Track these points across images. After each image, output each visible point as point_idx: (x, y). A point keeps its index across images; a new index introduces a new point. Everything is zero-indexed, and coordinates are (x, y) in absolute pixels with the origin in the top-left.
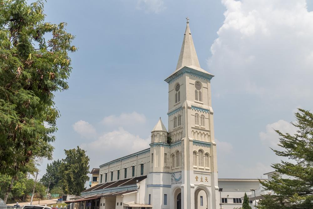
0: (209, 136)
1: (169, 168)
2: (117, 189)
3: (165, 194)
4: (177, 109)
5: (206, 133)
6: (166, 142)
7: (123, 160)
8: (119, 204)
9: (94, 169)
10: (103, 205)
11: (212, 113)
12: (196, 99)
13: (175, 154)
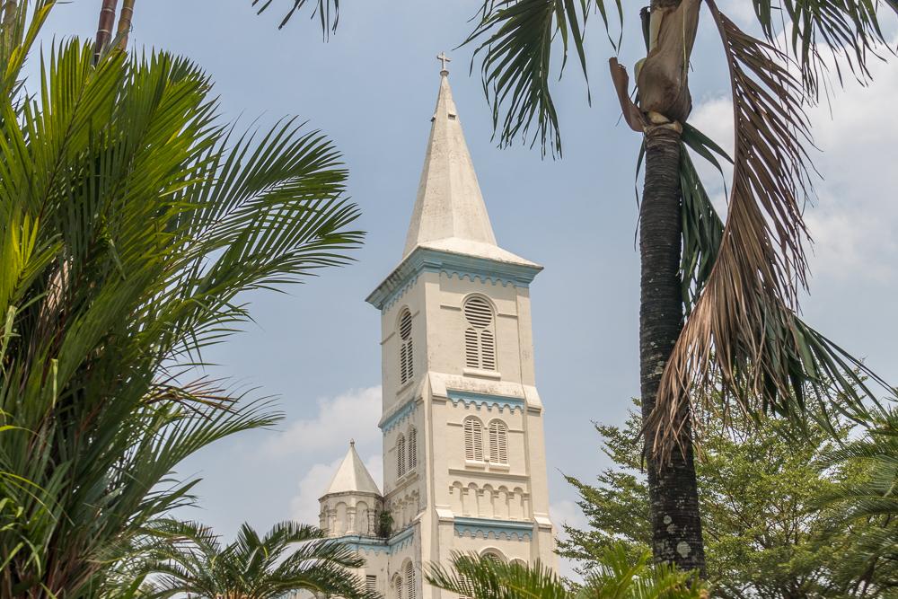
0: (526, 496)
4: (405, 407)
5: (511, 486)
6: (373, 534)
11: (535, 411)
12: (472, 362)
13: (403, 575)
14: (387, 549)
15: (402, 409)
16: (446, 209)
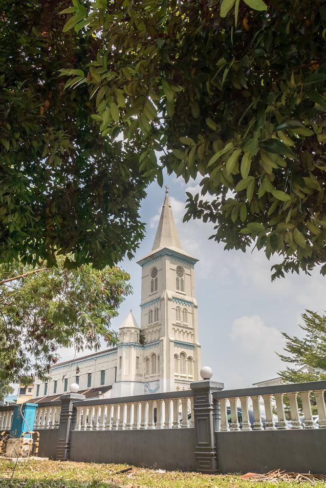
0: (193, 335)
4: (154, 300)
5: (189, 331)
6: (139, 342)
11: (196, 307)
12: (178, 288)
13: (150, 358)
15: (151, 301)
16: (169, 236)
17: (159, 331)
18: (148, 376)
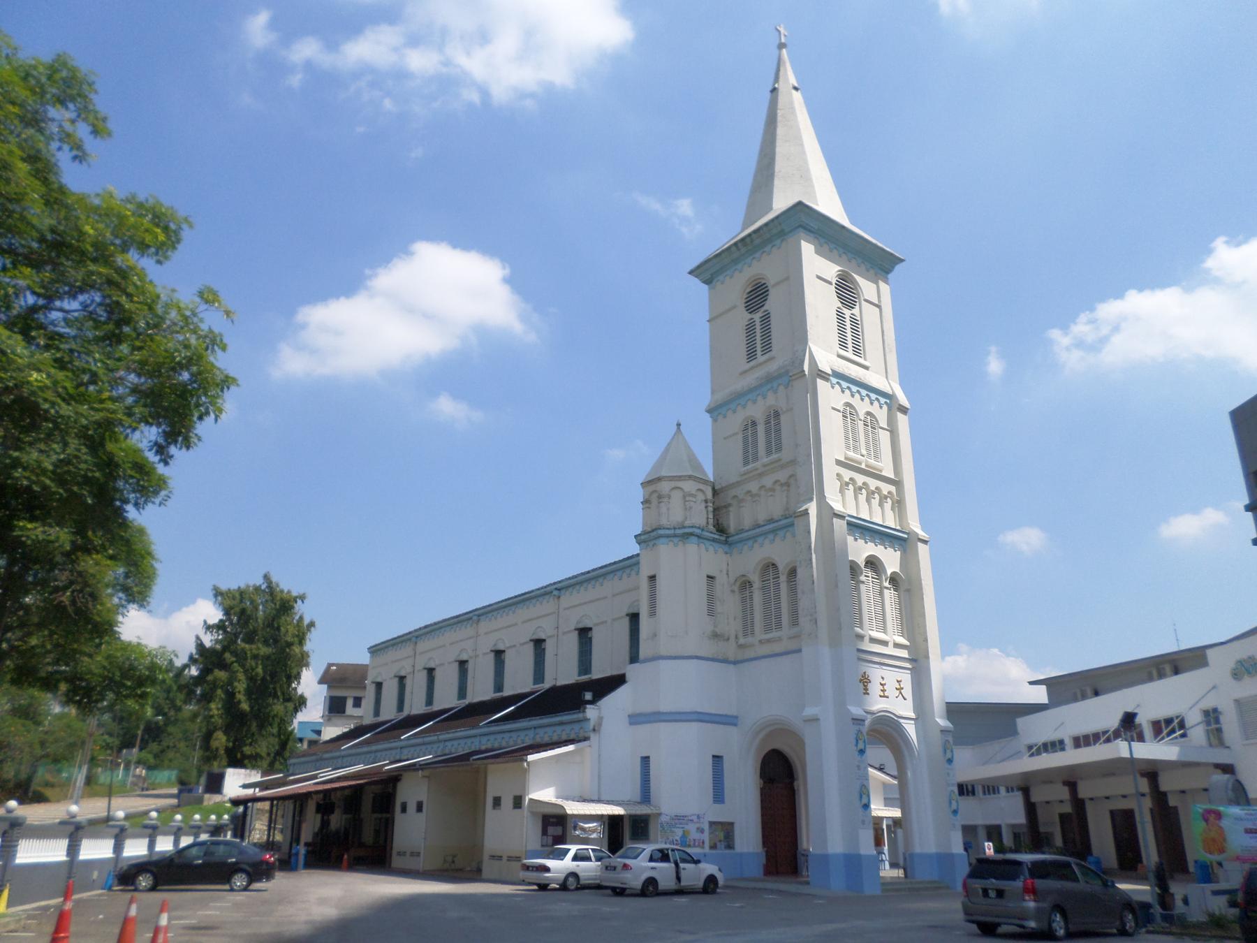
1: (728, 639)
2: (475, 736)
3: (714, 756)
6: (711, 527)
7: (482, 618)
8: (507, 802)
9: (333, 665)
10: (412, 807)
11: (903, 410)
12: (843, 345)
13: (755, 578)
14: (726, 548)
17: (787, 484)
18: (750, 640)
